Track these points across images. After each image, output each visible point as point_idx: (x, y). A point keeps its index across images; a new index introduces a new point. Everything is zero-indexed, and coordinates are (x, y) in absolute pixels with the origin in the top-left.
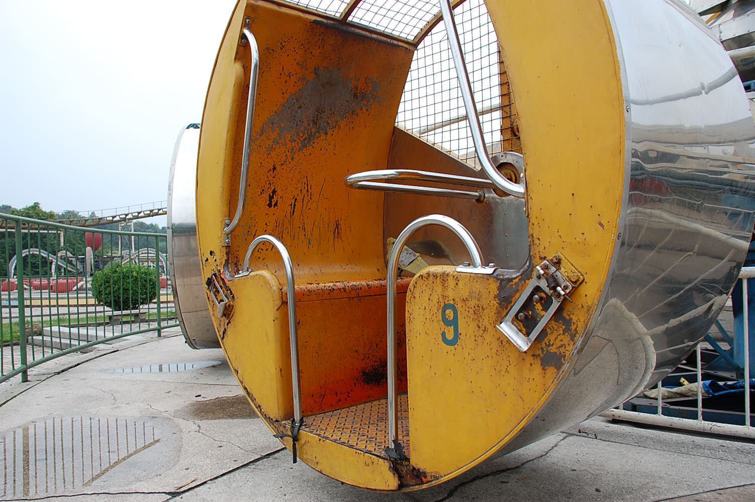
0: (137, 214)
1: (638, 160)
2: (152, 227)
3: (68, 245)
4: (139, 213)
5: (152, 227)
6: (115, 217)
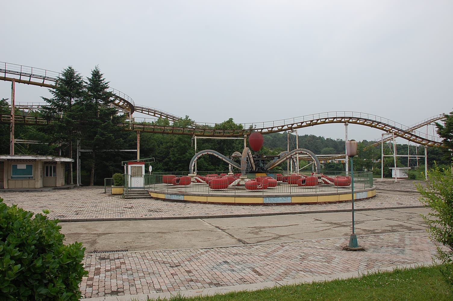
0: (281, 128)
1: (211, 152)
2: (320, 138)
3: (260, 151)
4: (302, 123)
5: (320, 138)
6: (284, 126)
